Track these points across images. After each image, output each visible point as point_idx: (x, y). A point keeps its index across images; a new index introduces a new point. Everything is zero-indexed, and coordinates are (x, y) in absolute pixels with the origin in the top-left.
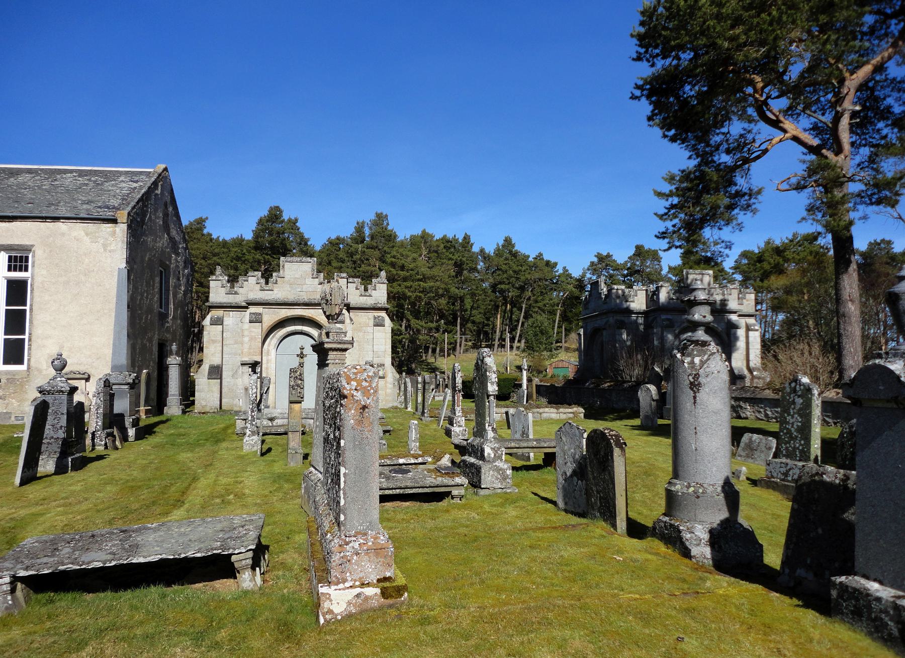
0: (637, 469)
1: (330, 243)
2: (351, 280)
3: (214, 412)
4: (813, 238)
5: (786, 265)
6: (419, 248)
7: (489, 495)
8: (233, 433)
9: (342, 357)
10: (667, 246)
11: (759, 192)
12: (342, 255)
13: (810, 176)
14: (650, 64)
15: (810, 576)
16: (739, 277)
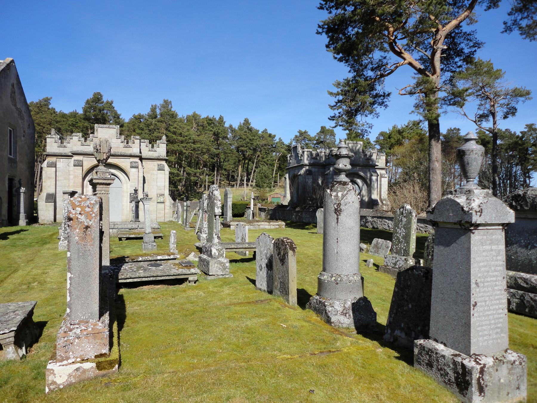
0: (310, 261)
1: (135, 118)
2: (142, 141)
3: (49, 224)
4: (417, 124)
5: (403, 140)
6: (192, 123)
7: (214, 280)
8: (56, 238)
9: (107, 189)
10: (334, 125)
11: (389, 95)
12: (142, 125)
13: (417, 87)
14: (328, 12)
15: (403, 335)
16: (378, 147)
